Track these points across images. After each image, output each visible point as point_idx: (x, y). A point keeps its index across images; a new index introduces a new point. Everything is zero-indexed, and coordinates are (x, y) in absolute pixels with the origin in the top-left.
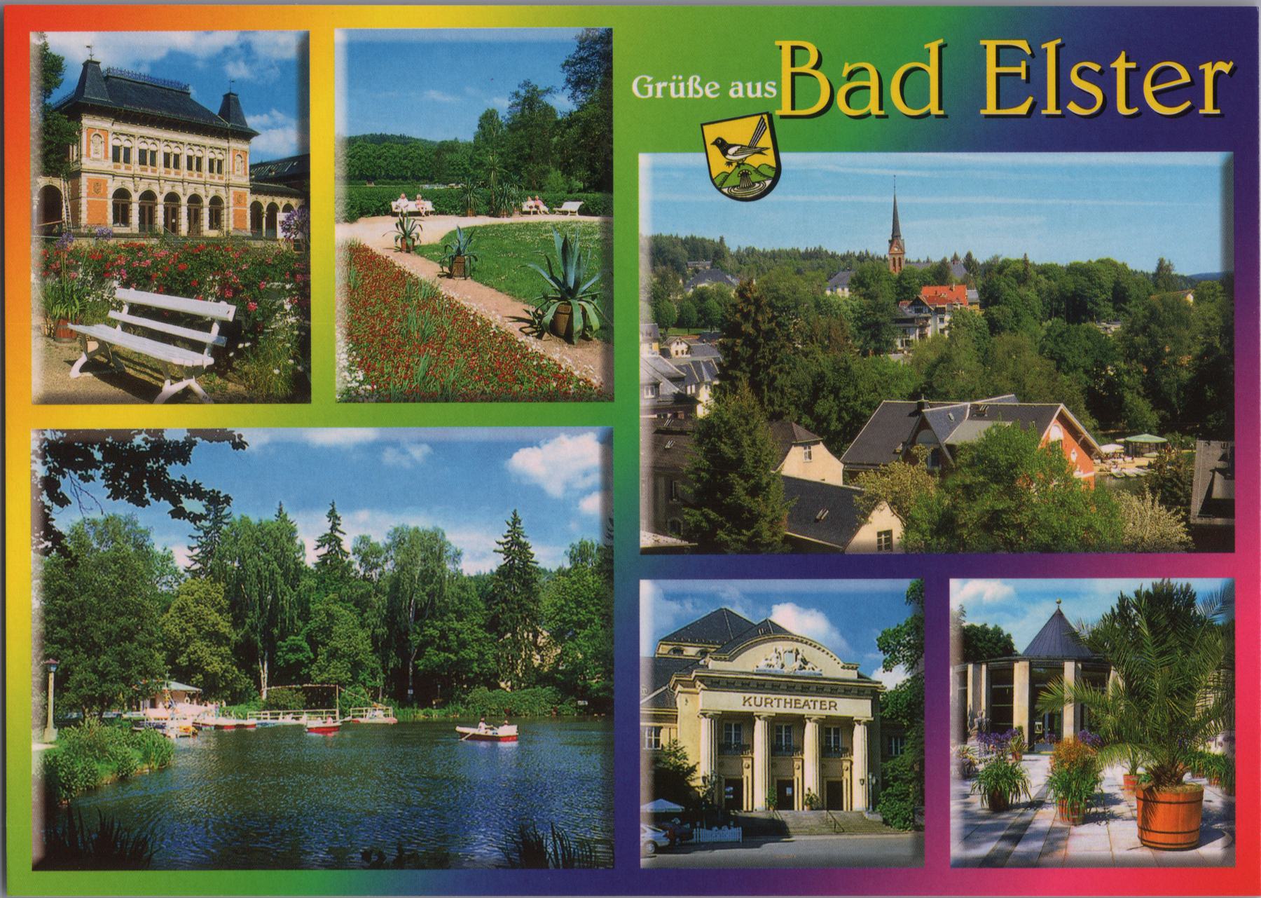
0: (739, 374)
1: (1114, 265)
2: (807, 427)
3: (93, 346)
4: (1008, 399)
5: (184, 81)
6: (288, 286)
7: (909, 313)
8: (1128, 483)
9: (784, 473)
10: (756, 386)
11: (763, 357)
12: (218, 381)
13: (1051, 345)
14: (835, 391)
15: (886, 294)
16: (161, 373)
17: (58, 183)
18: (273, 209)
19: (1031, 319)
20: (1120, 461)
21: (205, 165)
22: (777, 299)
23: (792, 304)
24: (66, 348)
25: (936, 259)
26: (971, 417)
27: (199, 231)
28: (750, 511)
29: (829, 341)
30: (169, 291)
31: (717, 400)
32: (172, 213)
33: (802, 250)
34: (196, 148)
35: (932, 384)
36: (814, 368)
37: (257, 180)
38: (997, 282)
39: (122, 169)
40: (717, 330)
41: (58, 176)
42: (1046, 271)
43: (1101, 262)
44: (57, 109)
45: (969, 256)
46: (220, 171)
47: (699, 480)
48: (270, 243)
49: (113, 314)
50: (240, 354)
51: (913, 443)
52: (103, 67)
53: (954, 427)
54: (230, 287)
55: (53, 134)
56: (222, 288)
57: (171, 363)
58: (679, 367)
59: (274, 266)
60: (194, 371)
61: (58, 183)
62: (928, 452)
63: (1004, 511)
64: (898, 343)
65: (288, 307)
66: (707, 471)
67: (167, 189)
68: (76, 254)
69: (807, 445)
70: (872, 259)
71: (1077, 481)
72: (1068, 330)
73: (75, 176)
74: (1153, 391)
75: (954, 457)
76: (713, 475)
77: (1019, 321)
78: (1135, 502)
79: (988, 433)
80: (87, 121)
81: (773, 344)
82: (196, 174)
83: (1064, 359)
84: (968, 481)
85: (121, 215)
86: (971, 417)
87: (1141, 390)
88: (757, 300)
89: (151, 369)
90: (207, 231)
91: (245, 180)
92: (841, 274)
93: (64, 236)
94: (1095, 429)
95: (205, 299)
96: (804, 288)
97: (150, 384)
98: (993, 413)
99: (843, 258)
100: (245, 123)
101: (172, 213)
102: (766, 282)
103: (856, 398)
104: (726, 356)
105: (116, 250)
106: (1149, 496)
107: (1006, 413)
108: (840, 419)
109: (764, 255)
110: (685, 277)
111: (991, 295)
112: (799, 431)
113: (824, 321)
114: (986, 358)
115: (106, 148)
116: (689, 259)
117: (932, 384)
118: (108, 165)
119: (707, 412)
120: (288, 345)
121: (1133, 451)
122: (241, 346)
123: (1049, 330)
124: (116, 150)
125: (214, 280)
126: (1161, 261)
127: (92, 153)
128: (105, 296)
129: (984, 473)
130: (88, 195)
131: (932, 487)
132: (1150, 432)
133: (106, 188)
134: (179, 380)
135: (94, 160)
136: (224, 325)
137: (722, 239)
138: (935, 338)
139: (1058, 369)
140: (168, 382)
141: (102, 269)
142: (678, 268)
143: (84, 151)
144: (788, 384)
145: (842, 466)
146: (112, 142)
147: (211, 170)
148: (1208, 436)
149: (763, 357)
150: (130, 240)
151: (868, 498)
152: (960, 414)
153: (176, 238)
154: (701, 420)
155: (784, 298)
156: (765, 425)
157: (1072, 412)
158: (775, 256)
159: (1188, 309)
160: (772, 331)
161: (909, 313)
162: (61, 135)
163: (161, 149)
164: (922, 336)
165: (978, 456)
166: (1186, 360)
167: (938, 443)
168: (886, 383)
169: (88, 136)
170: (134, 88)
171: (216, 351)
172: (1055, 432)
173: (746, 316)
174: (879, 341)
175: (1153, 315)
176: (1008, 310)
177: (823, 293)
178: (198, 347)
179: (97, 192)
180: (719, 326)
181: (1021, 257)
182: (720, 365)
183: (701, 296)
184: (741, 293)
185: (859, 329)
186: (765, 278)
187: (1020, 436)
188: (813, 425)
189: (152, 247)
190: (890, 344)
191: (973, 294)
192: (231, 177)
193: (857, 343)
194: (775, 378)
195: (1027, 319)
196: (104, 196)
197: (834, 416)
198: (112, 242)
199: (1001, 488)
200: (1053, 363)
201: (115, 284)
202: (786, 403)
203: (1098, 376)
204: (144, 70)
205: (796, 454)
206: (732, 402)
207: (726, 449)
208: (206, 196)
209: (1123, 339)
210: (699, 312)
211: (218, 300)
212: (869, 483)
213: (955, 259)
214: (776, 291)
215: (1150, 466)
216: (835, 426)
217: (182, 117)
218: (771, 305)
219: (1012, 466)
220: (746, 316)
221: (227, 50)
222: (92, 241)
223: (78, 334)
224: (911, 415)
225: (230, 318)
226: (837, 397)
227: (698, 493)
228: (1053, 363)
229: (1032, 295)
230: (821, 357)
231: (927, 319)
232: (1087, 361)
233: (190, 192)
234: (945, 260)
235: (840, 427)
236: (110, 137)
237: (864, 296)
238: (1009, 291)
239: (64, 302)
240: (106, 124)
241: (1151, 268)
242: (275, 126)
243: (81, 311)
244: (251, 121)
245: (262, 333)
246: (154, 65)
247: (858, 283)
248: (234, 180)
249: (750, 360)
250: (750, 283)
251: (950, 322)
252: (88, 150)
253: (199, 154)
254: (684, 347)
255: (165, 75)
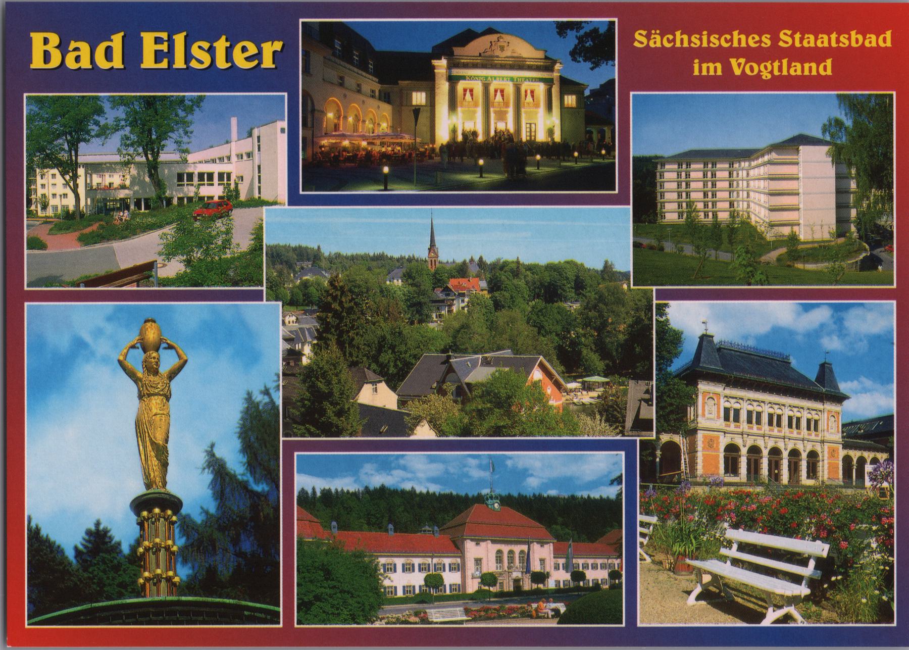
0: (330, 336)
1: (575, 264)
2: (374, 371)
3: (707, 578)
4: (507, 353)
5: (786, 353)
6: (874, 528)
7: (442, 296)
8: (585, 409)
9: (359, 401)
10: (341, 344)
11: (346, 325)
12: (814, 608)
13: (535, 317)
14: (393, 347)
15: (427, 284)
16: (765, 602)
17: (678, 439)
18: (862, 461)
19: (521, 300)
20: (579, 394)
21: (785, 421)
22: (355, 287)
23: (365, 290)
24: (684, 580)
25: (459, 260)
26: (482, 365)
27: (798, 481)
28: (337, 427)
29: (388, 315)
30: (772, 531)
31: (316, 354)
32: (775, 465)
33: (371, 254)
34: (776, 407)
35: (457, 342)
36: (379, 332)
37: (849, 436)
38: (499, 276)
39: (732, 427)
40: (316, 308)
41: (678, 433)
42: (531, 268)
43: (567, 262)
44: (676, 376)
45: (481, 258)
46: (816, 429)
47: (304, 406)
48: (859, 491)
49: (724, 551)
50: (833, 585)
51: (444, 382)
52: (716, 340)
53: (471, 371)
54: (825, 528)
55: (674, 397)
56: (817, 530)
57: (774, 593)
58: (290, 332)
59: (863, 511)
60: (793, 600)
61: (678, 439)
62: (453, 388)
63: (504, 427)
64: (434, 316)
65: (874, 545)
66: (309, 400)
67: (771, 444)
68: (692, 500)
69: (374, 383)
70: (417, 261)
71: (551, 407)
72: (546, 308)
73: (691, 433)
74: (602, 349)
75: (471, 391)
76: (313, 403)
77: (513, 302)
78: (588, 420)
79: (493, 375)
80: (703, 387)
81: (352, 317)
82: (795, 431)
83: (543, 327)
84: (480, 407)
85: (732, 466)
86: (482, 365)
87: (593, 347)
88: (342, 287)
89: (756, 598)
90: (805, 481)
91: (838, 437)
92: (396, 271)
93: (683, 485)
94: (563, 373)
95: (803, 538)
96: (372, 278)
97: (756, 611)
98: (497, 362)
99: (398, 260)
100: (837, 387)
101: (775, 465)
102: (347, 276)
103: (406, 352)
104: (322, 324)
105: (727, 496)
106: (598, 417)
107: (506, 362)
108: (396, 366)
109: (347, 258)
110: (295, 272)
111: (495, 284)
112: (370, 374)
113: (384, 301)
114: (492, 326)
115: (719, 408)
116: (298, 261)
117: (457, 342)
118: (720, 424)
119: (309, 361)
120: (875, 578)
121: (587, 387)
122: (833, 579)
123: (533, 307)
124: (727, 410)
125: (811, 523)
126: (606, 262)
127: (706, 413)
128: (717, 535)
129: (491, 402)
130: (703, 449)
131: (456, 410)
132: (599, 375)
133: (718, 443)
134: (780, 607)
135: (708, 419)
136: (820, 562)
137: (319, 247)
138: (458, 313)
139: (539, 333)
140: (771, 609)
141: (715, 512)
142: (290, 266)
143: (700, 412)
144: (362, 342)
145: (397, 397)
146: (724, 404)
147: (809, 428)
148: (637, 377)
149: (346, 325)
150: (739, 488)
151: (414, 418)
152: (474, 364)
153: (778, 487)
154: (305, 367)
155: (359, 286)
156: (347, 370)
157: (548, 361)
158: (353, 258)
159: (624, 293)
160: (352, 308)
161: (442, 296)
162: (680, 398)
163: (766, 410)
164: (450, 311)
165: (487, 391)
166: (622, 327)
167: (459, 381)
168: (426, 342)
169: (704, 399)
170: (742, 357)
171: (812, 583)
172: (537, 375)
173: (335, 298)
174: (421, 315)
175: (601, 298)
176: (507, 294)
177: (385, 283)
178: (796, 579)
179: (711, 446)
180: (317, 305)
181: (515, 260)
182: (317, 330)
183: (305, 285)
184: (331, 283)
185: (409, 307)
186: (347, 273)
187: (514, 376)
188: (378, 370)
189: (758, 494)
190: (428, 316)
191: (483, 284)
192: (826, 433)
193: (407, 316)
194: (353, 339)
195: (519, 300)
196: (717, 450)
197: (392, 364)
198: (723, 489)
199: (502, 411)
200: (536, 329)
201: (726, 525)
202: (360, 356)
203: (565, 338)
204: (751, 343)
205: (367, 389)
206: (325, 354)
207: (321, 385)
208: (804, 450)
209: (581, 314)
210: (304, 295)
211: (814, 540)
212: (414, 408)
213: (472, 260)
214: (354, 281)
215: (599, 397)
216: (392, 370)
217: (782, 383)
218: (350, 291)
219: (509, 397)
220: (335, 298)
221: (822, 326)
222: (707, 489)
223: (694, 568)
224: (442, 363)
225: (825, 555)
226: (393, 352)
227: (302, 414)
228: (536, 329)
229: (521, 283)
230: (383, 324)
231: (453, 300)
232: (559, 328)
233: (790, 446)
234: (465, 261)
235: (395, 371)
236: (722, 400)
237: (412, 285)
238: (508, 282)
239: (682, 541)
240: (718, 389)
241: (599, 267)
242: (865, 390)
243: (697, 549)
244: (844, 387)
245: (851, 567)
246: (758, 338)
247: (408, 276)
248: (828, 437)
249: (337, 327)
250: (337, 276)
251: (468, 302)
252: (704, 410)
253: (798, 415)
254: (294, 318)
255: (776, 348)
